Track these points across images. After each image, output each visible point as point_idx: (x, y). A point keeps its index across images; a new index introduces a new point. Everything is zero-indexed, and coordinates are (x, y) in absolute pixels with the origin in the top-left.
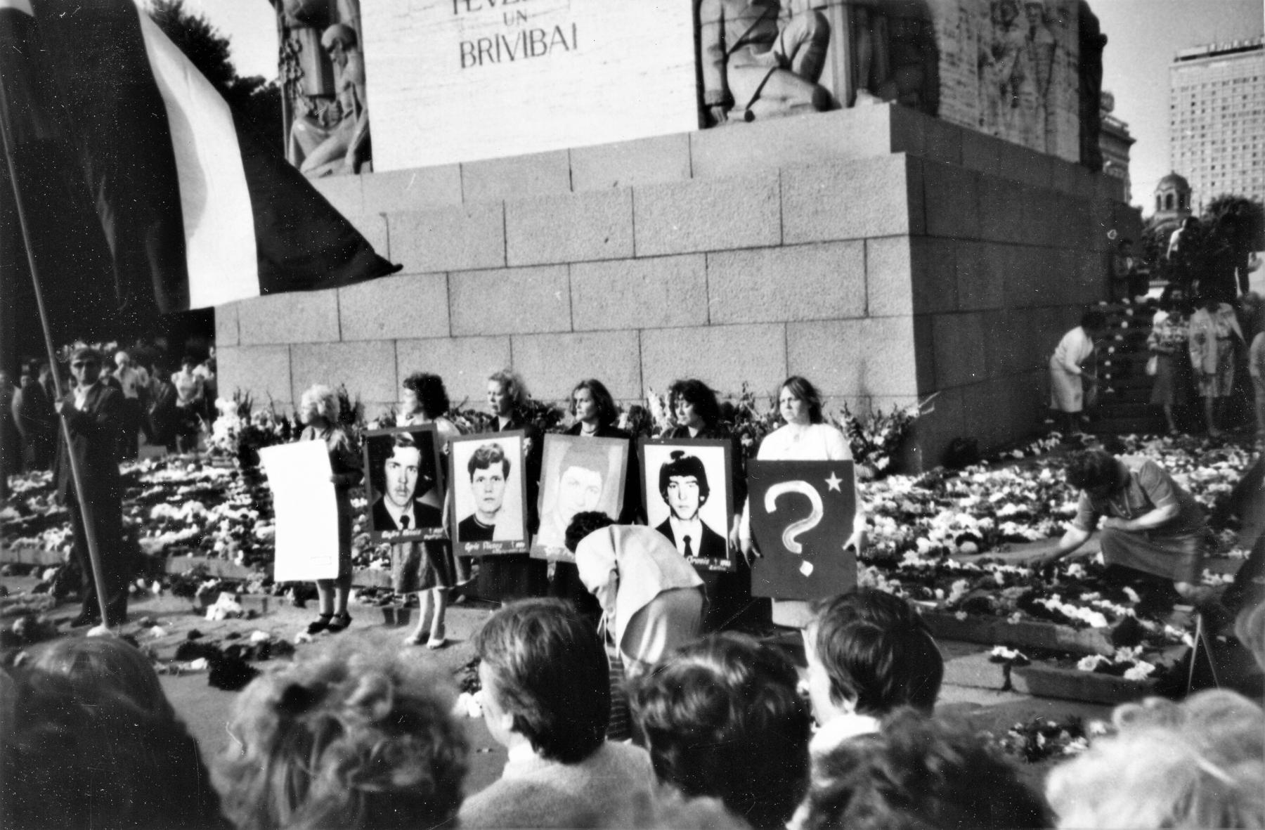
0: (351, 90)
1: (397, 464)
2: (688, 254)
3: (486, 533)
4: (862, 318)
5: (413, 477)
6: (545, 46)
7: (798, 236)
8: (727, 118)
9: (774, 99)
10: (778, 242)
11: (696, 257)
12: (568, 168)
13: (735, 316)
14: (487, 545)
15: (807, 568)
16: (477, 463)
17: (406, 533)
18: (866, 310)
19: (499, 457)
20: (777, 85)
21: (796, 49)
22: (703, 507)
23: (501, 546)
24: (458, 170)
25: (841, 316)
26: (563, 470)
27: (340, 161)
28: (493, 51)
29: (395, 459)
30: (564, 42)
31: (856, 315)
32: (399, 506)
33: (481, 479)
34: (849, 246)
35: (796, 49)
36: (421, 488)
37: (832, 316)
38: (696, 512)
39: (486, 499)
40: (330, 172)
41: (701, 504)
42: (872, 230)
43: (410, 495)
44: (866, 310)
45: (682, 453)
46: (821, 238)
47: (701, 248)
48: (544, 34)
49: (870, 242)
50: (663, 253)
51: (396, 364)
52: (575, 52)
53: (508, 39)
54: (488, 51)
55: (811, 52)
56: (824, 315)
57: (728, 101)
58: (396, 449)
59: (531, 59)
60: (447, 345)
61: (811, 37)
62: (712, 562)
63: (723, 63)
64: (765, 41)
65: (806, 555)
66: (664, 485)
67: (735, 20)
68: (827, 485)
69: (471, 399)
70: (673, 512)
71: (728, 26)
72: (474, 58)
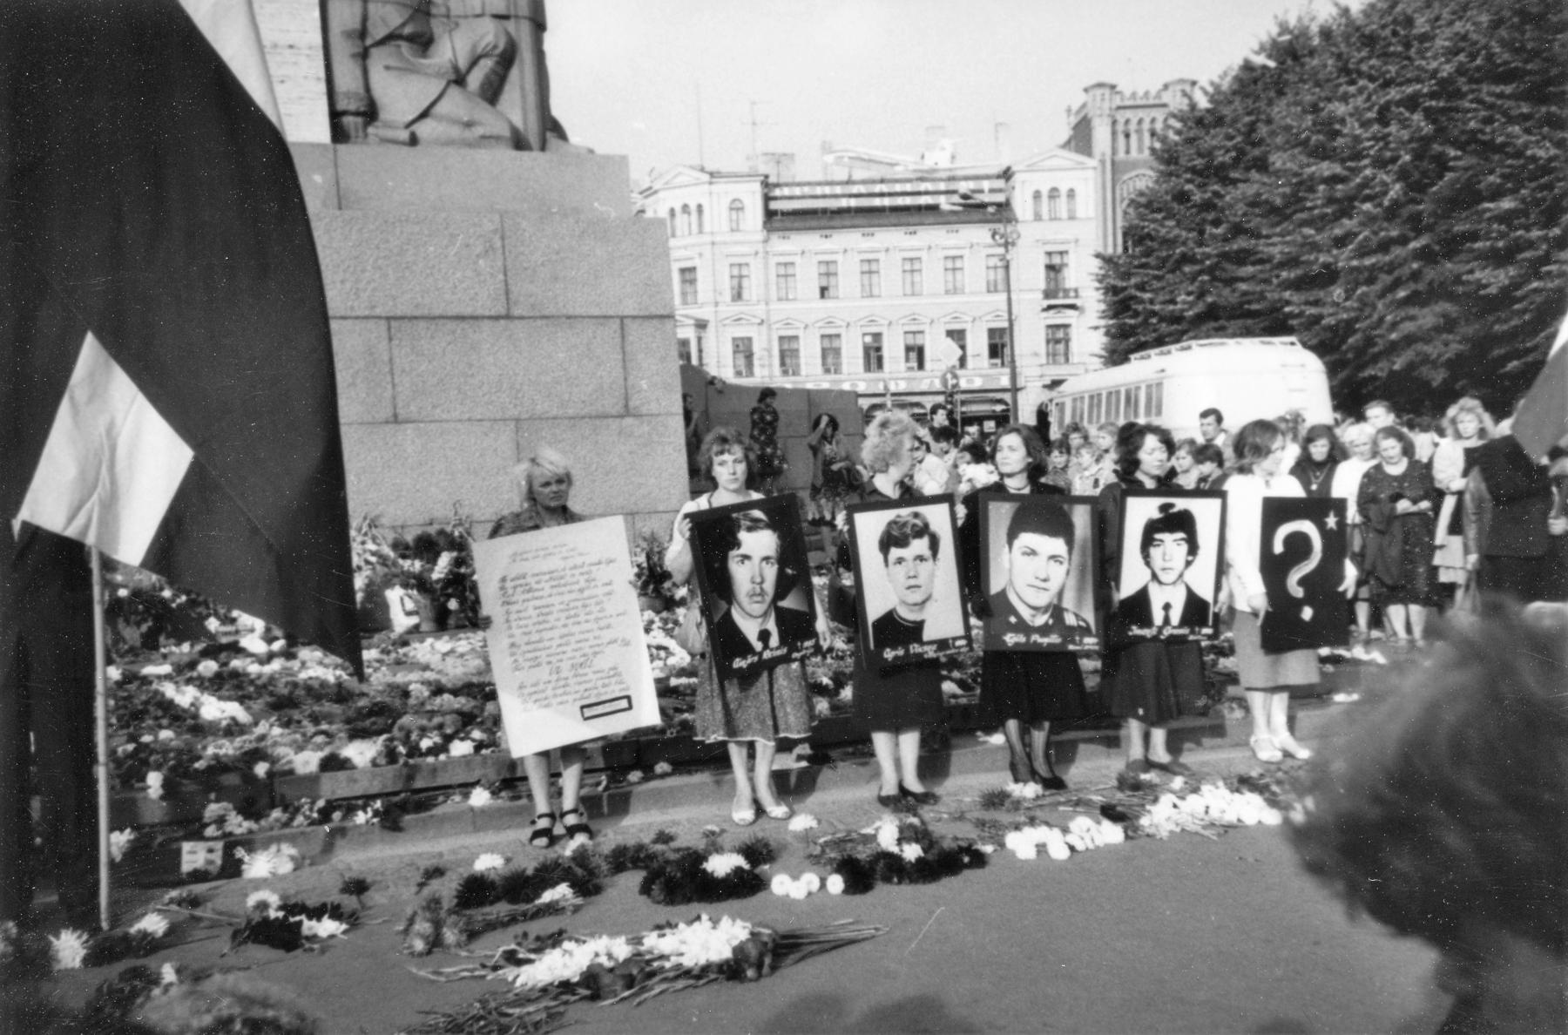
1: (746, 557)
2: (357, 318)
3: (914, 631)
4: (621, 416)
5: (771, 572)
7: (533, 306)
8: (366, 135)
9: (455, 121)
11: (371, 324)
13: (438, 411)
14: (915, 648)
15: (1307, 613)
16: (891, 540)
17: (767, 655)
18: (626, 406)
19: (923, 530)
20: (455, 104)
21: (474, 63)
22: (1192, 568)
23: (934, 647)
25: (594, 413)
26: (1012, 536)
29: (742, 551)
31: (614, 412)
32: (756, 617)
33: (900, 561)
35: (474, 63)
36: (783, 588)
37: (583, 413)
38: (1181, 576)
39: (909, 588)
41: (1188, 564)
42: (629, 308)
43: (769, 598)
44: (626, 406)
45: (1171, 506)
55: (493, 71)
56: (571, 412)
57: (370, 113)
58: (743, 535)
61: (498, 51)
62: (1193, 632)
64: (423, 42)
65: (1308, 600)
66: (1148, 541)
68: (1325, 524)
70: (1155, 577)
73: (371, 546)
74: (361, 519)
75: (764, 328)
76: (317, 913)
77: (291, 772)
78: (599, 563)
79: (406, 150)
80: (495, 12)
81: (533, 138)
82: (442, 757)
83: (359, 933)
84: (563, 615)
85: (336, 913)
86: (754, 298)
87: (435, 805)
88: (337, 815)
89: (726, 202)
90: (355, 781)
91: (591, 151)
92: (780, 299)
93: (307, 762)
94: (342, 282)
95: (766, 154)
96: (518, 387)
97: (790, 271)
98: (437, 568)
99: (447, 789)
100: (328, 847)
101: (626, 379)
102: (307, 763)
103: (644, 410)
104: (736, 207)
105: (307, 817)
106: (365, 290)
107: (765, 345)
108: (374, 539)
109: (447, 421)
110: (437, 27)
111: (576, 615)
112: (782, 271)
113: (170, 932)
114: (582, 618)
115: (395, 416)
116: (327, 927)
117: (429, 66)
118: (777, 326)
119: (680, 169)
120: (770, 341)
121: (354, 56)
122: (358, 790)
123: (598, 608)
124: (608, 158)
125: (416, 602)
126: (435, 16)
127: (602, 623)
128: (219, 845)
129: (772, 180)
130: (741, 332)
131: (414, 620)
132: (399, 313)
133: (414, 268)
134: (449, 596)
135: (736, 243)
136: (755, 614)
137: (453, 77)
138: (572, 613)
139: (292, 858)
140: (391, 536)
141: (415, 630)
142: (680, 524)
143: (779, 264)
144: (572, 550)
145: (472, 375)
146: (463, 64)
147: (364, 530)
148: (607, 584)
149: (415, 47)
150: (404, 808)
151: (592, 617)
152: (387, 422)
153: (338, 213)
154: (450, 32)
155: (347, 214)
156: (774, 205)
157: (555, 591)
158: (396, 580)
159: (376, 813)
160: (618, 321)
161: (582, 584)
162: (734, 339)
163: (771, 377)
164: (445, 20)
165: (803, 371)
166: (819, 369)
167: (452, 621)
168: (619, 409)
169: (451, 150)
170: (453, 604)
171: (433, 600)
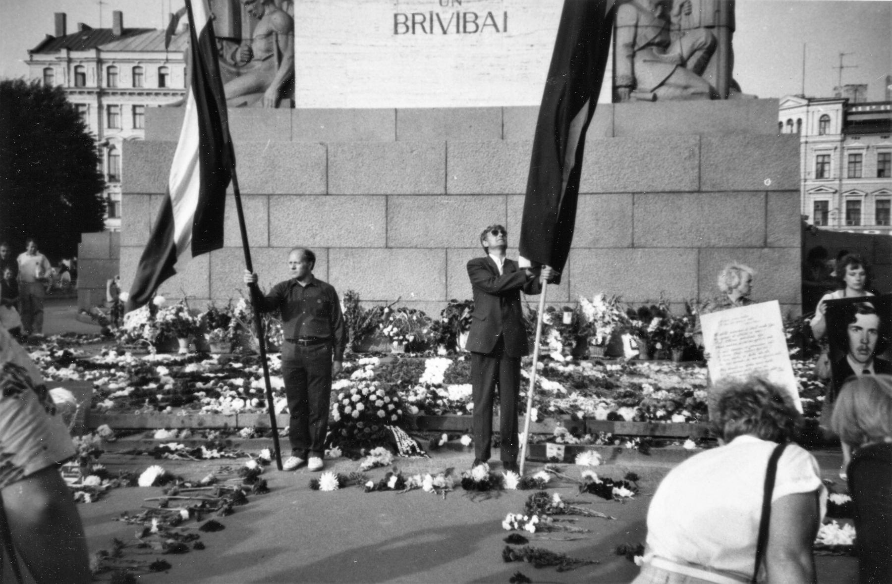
0: (274, 37)
1: (859, 328)
2: (617, 193)
4: (762, 248)
5: (873, 338)
6: (477, 26)
7: (714, 186)
8: (629, 97)
9: (678, 86)
10: (696, 188)
11: (625, 195)
12: (501, 123)
13: (656, 242)
18: (765, 242)
20: (680, 77)
21: (692, 54)
24: (393, 114)
25: (745, 245)
27: (257, 95)
28: (427, 25)
29: (857, 324)
30: (495, 25)
31: (758, 244)
34: (754, 195)
35: (692, 54)
40: (245, 104)
46: (732, 188)
47: (630, 189)
48: (476, 17)
49: (769, 193)
50: (595, 191)
51: (328, 268)
52: (505, 34)
53: (441, 17)
54: (422, 24)
55: (702, 57)
57: (633, 85)
58: (859, 316)
59: (462, 35)
60: (381, 254)
61: (706, 46)
63: (632, 56)
64: (664, 46)
67: (647, 27)
69: (403, 298)
71: (640, 30)
72: (407, 27)
73: (615, 312)
74: (611, 298)
75: (837, 195)
76: (619, 485)
77: (594, 418)
78: (765, 326)
79: (650, 104)
80: (707, 24)
81: (722, 92)
82: (669, 422)
83: (640, 498)
84: (747, 354)
85: (627, 486)
86: (832, 176)
87: (666, 445)
88: (617, 442)
89: (817, 117)
90: (625, 427)
91: (756, 97)
92: (849, 178)
93: (601, 414)
94: (612, 175)
95: (847, 85)
96: (701, 230)
97: (858, 159)
98: (651, 326)
99: (672, 438)
100: (614, 457)
101: (766, 227)
102: (601, 414)
103: (776, 245)
104: (825, 120)
105: (602, 440)
106: (623, 179)
107: (837, 206)
108: (617, 308)
109: (659, 248)
110: (673, 37)
111: (754, 354)
112: (853, 159)
113: (551, 481)
114: (757, 355)
115: (633, 244)
116: (623, 492)
117: (667, 58)
118: (847, 194)
119: (789, 98)
120: (840, 204)
121: (628, 57)
122: (625, 431)
123: (765, 350)
124: (766, 101)
125: (638, 343)
126: (672, 31)
127: (768, 359)
128: (563, 447)
129: (851, 101)
130: (821, 197)
131: (636, 352)
132: (639, 190)
133: (650, 166)
134: (656, 342)
135: (823, 142)
136: (860, 360)
137: (679, 62)
138: (751, 353)
139: (599, 459)
140: (626, 307)
141: (637, 357)
142: (821, 305)
143: (850, 155)
144: (751, 319)
145: (676, 223)
146: (685, 55)
147: (613, 303)
148: (769, 337)
149: (660, 48)
150: (650, 444)
151: (762, 355)
152: (628, 247)
153: (612, 138)
154: (680, 38)
155: (617, 139)
156: (851, 118)
157: (743, 341)
158: (627, 331)
159: (637, 444)
160: (764, 194)
161: (757, 337)
162: (816, 202)
163: (840, 226)
164: (677, 32)
165: (862, 222)
166: (873, 222)
167: (656, 355)
168: (761, 243)
169: (674, 102)
170: (659, 346)
171: (648, 343)
